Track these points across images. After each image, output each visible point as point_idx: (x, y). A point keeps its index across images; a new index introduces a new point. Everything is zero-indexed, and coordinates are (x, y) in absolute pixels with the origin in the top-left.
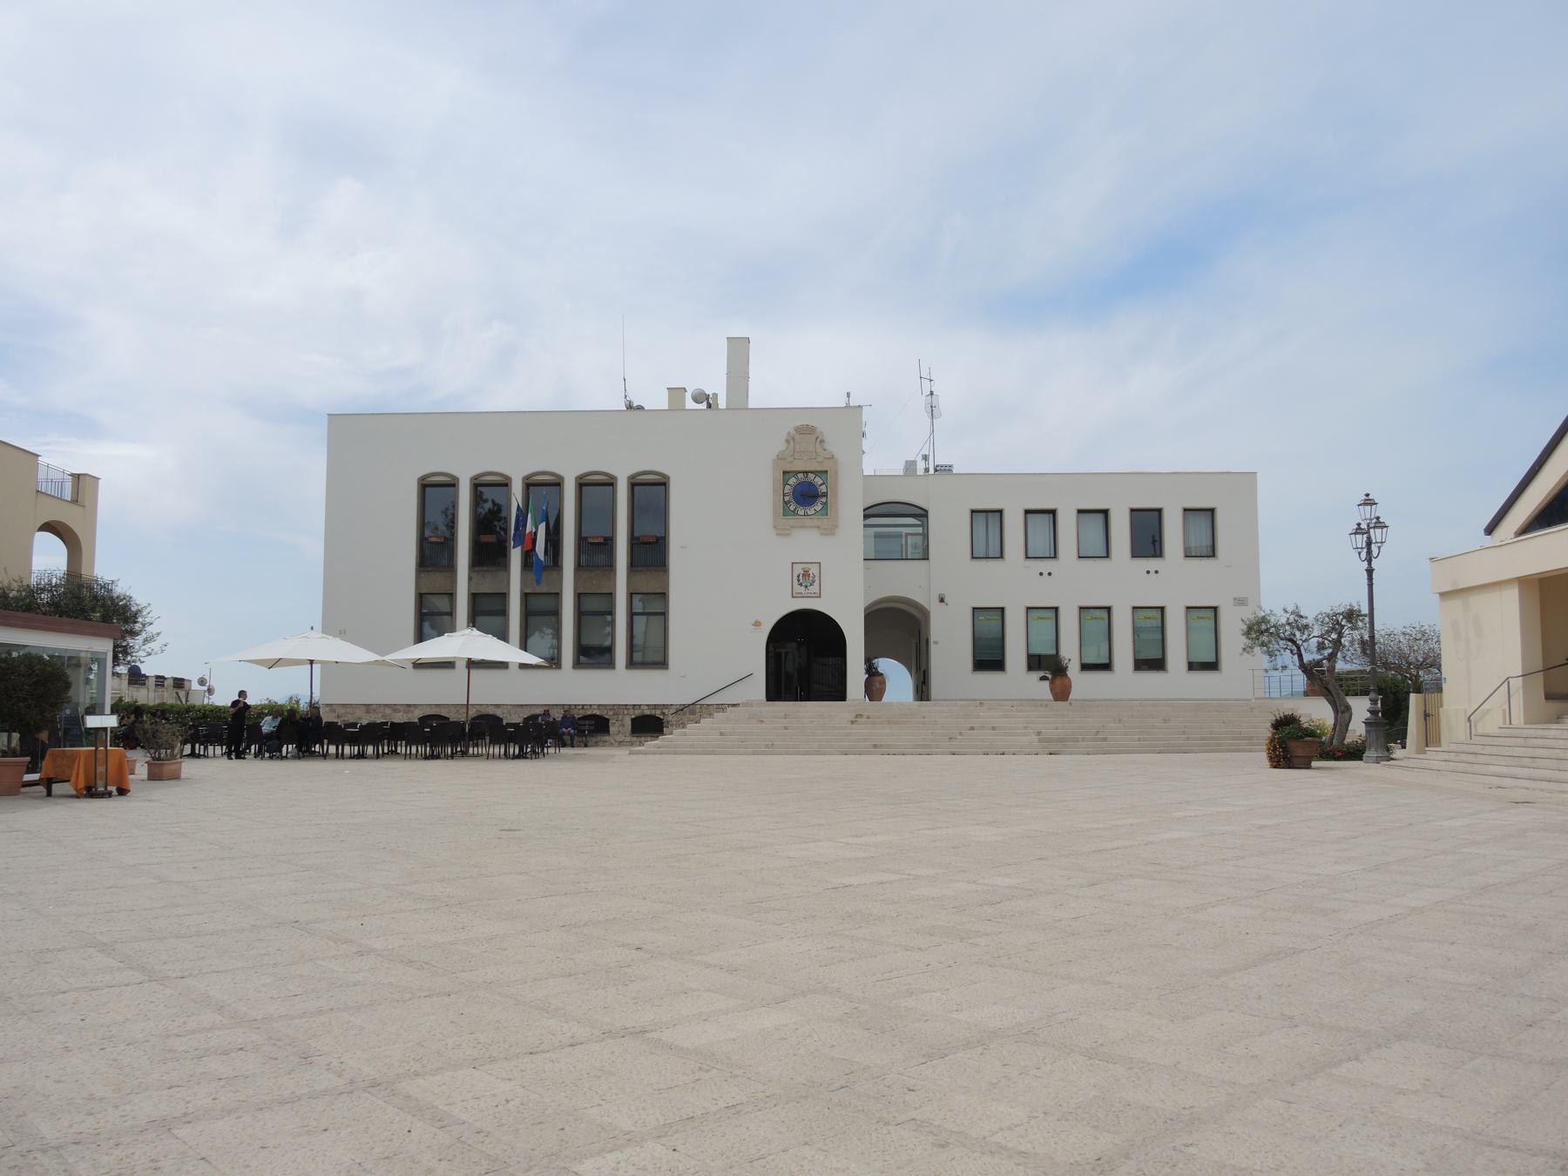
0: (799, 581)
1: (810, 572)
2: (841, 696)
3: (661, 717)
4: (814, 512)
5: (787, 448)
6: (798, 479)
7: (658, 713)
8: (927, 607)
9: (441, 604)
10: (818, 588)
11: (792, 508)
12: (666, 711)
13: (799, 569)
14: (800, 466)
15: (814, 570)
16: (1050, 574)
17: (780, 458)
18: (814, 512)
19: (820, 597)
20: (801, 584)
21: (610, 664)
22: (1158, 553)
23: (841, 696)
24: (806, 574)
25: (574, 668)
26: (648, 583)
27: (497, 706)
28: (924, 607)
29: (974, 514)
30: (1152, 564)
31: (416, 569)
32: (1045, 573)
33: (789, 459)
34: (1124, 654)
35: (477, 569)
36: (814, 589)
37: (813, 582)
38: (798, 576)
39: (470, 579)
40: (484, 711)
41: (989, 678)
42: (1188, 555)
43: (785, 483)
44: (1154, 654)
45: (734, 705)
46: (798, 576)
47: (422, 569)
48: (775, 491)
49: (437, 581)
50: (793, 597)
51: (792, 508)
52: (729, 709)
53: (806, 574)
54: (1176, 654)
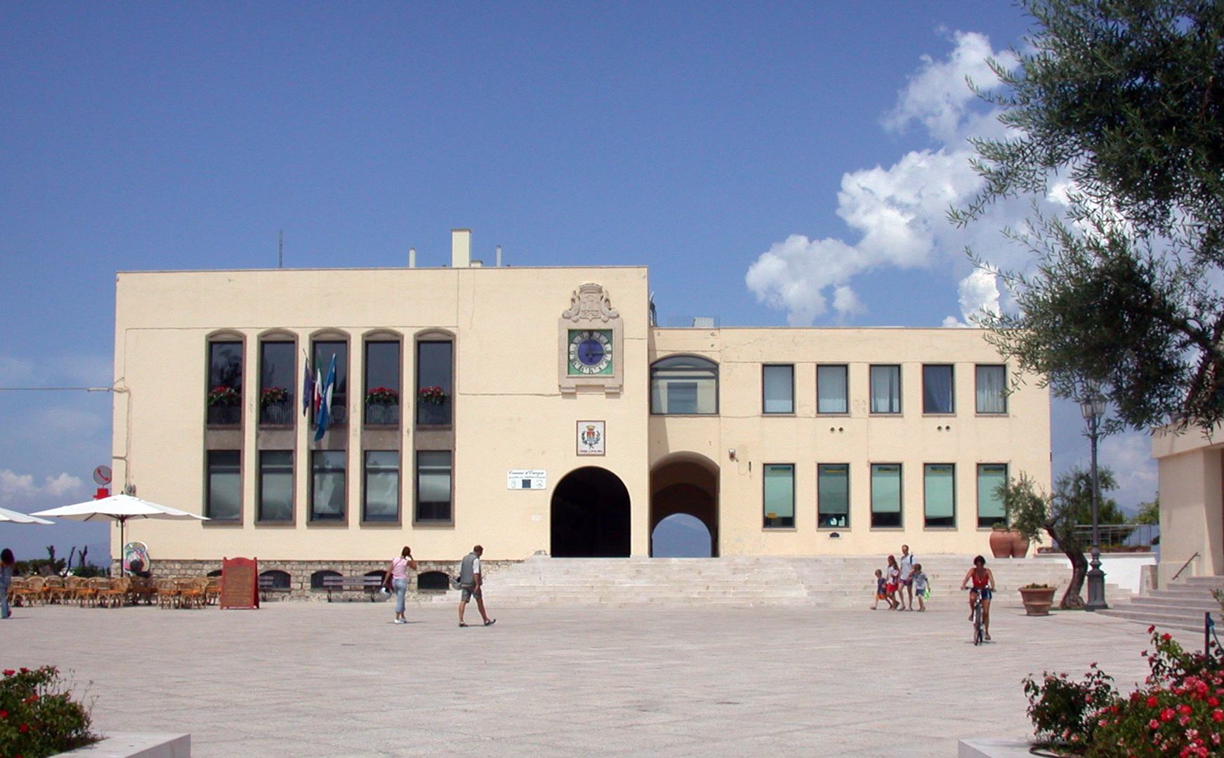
0: (583, 438)
1: (595, 430)
2: (626, 553)
3: (447, 573)
4: (598, 370)
5: (572, 307)
6: (583, 337)
7: (444, 569)
8: (718, 464)
9: (332, 461)
10: (603, 445)
11: (577, 366)
12: (452, 567)
13: (583, 428)
14: (585, 325)
15: (598, 428)
16: (948, 428)
17: (566, 317)
18: (598, 370)
19: (604, 455)
20: (586, 443)
21: (238, 522)
22: (896, 408)
23: (626, 553)
24: (591, 432)
25: (361, 525)
26: (433, 440)
27: (441, 563)
28: (715, 464)
29: (765, 368)
30: (943, 421)
31: (204, 426)
32: (837, 429)
33: (575, 318)
34: (807, 511)
35: (264, 426)
36: (598, 447)
37: (598, 440)
38: (583, 434)
39: (258, 436)
40: (273, 567)
41: (780, 536)
42: (978, 413)
43: (570, 342)
44: (890, 507)
45: (519, 561)
46: (583, 434)
47: (210, 426)
48: (560, 350)
49: (224, 439)
50: (578, 455)
51: (577, 366)
52: (514, 565)
53: (591, 432)
54: (860, 511)
